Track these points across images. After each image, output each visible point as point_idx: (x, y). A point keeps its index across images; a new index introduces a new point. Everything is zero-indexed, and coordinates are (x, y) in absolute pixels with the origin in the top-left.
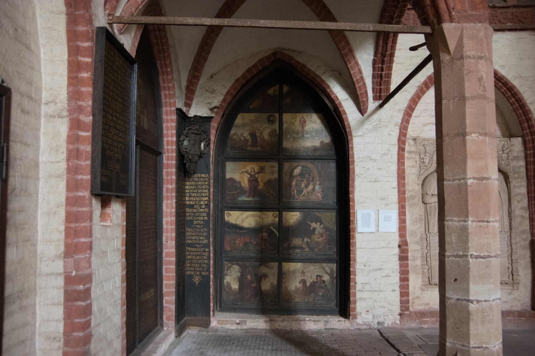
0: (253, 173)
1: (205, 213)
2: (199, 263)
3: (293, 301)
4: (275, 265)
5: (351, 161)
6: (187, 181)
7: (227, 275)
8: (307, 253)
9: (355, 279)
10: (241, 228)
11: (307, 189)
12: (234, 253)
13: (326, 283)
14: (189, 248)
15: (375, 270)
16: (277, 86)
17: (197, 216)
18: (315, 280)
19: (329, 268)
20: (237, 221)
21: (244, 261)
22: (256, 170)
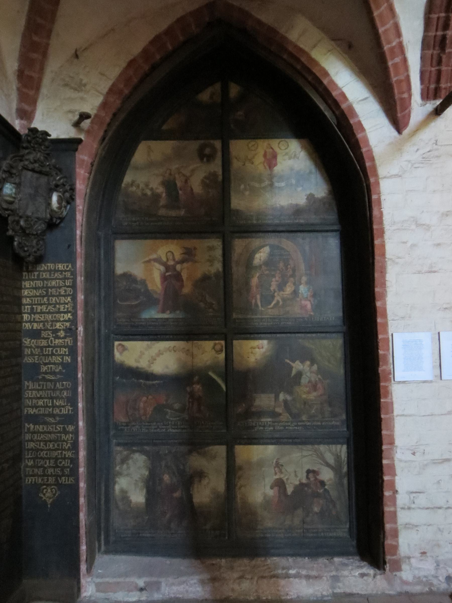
0: (171, 263)
1: (65, 347)
2: (53, 459)
3: (259, 527)
4: (221, 450)
5: (377, 229)
6: (25, 280)
8: (287, 424)
9: (392, 483)
11: (282, 293)
12: (134, 429)
13: (326, 487)
14: (32, 426)
15: (435, 462)
16: (218, 86)
17: (48, 355)
18: (304, 481)
19: (333, 454)
20: (139, 362)
21: (155, 445)
22: (178, 255)
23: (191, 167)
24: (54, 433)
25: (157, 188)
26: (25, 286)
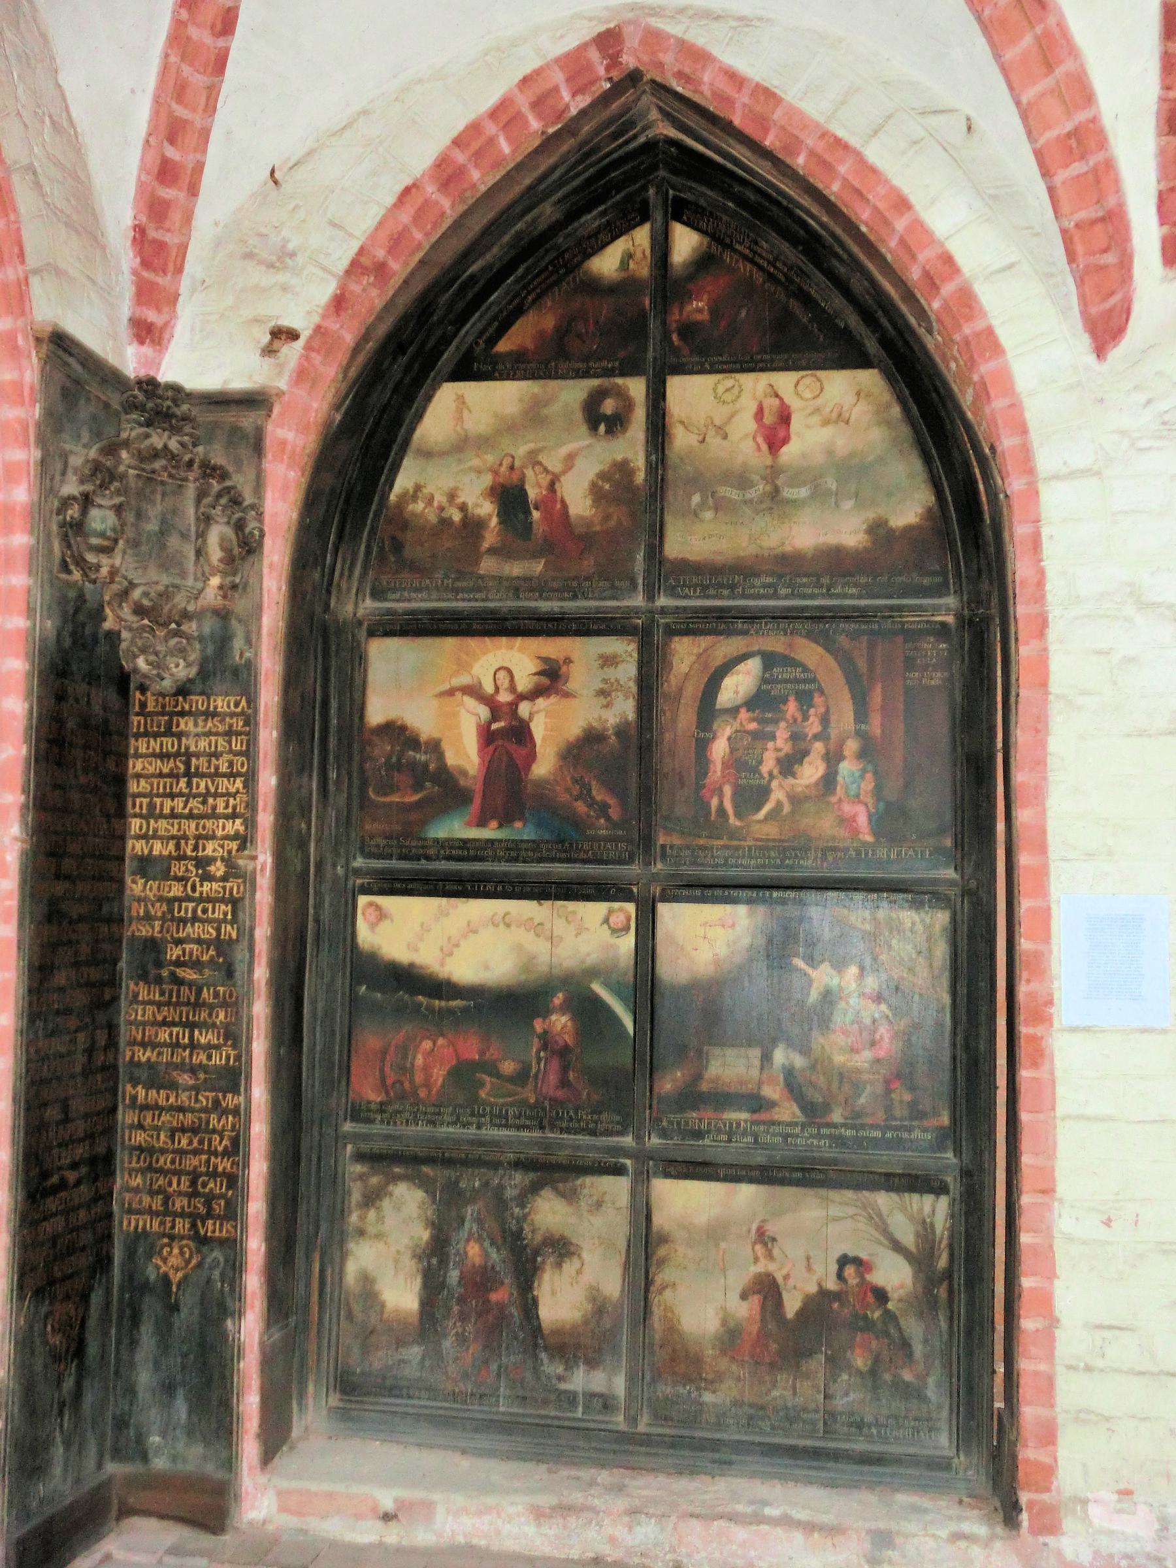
0: (504, 697)
1: (222, 900)
2: (188, 1173)
7: (361, 1233)
8: (789, 1130)
9: (1046, 1301)
10: (440, 988)
11: (791, 780)
13: (890, 1306)
14: (141, 1092)
18: (832, 1285)
19: (911, 1218)
20: (417, 950)
23: (564, 451)
24: (193, 1111)
25: (477, 505)
26: (137, 749)
